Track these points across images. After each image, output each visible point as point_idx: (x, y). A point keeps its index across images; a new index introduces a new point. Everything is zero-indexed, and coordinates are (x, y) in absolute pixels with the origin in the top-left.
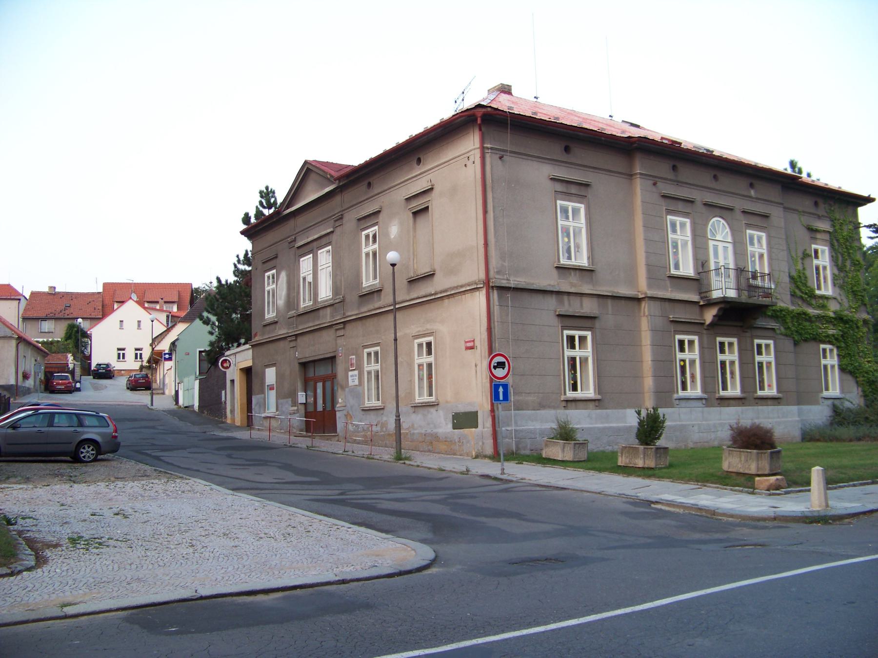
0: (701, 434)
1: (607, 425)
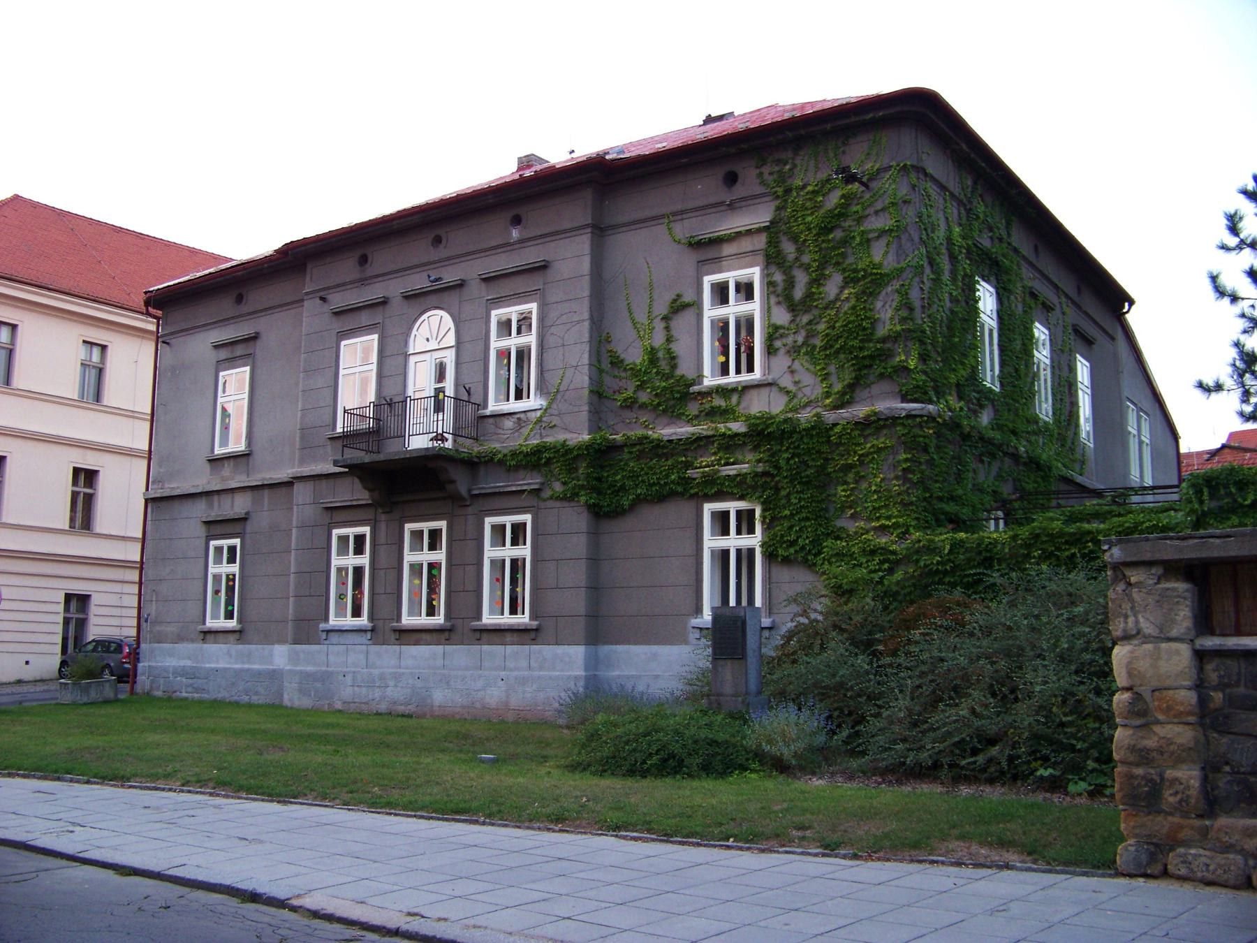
0: (356, 689)
1: (247, 666)
